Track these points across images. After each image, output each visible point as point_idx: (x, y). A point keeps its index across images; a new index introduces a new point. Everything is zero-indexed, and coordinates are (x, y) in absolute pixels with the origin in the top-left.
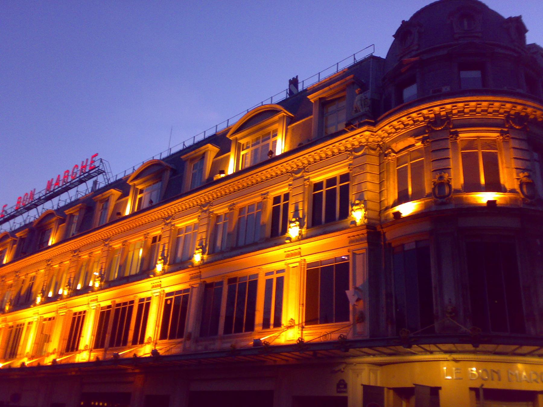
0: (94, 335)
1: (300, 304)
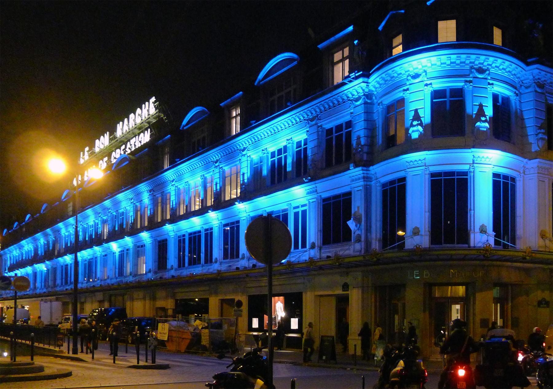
1: (219, 249)
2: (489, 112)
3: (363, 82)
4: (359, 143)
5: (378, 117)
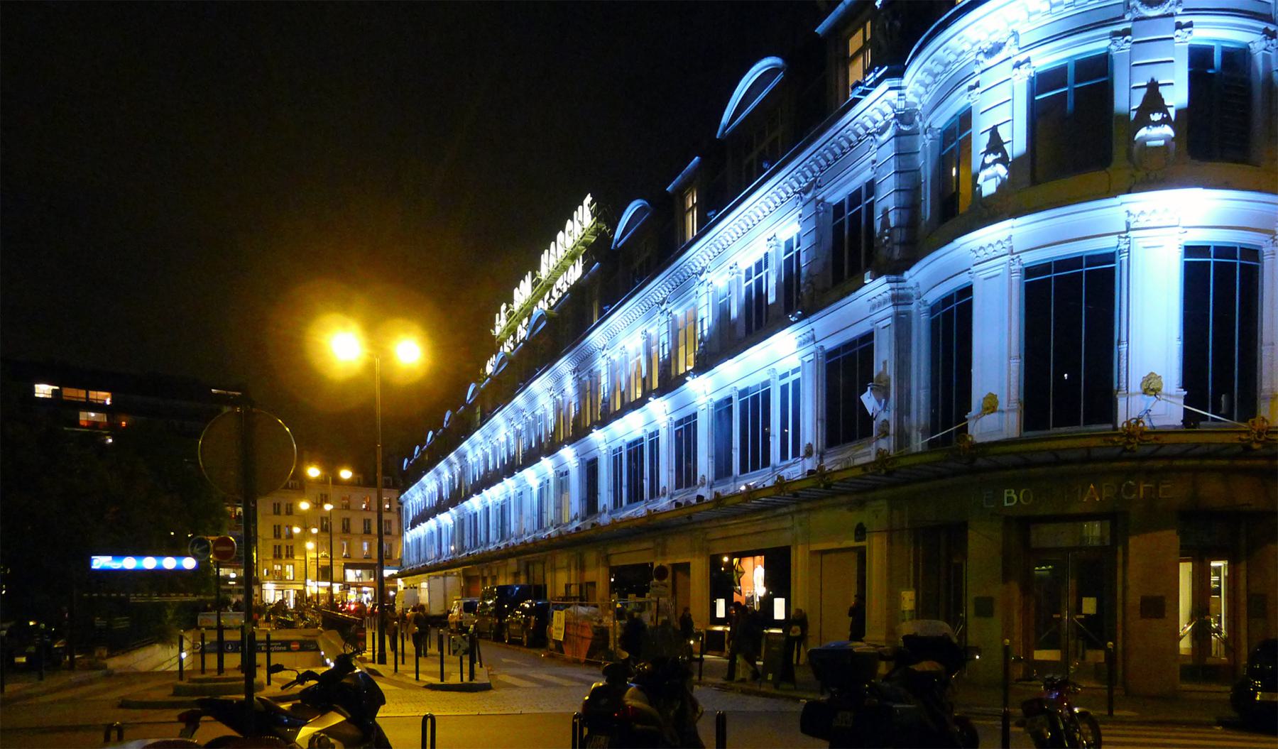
0: (611, 491)
1: (669, 470)
2: (1177, 96)
3: (891, 89)
4: (885, 223)
5: (925, 163)
